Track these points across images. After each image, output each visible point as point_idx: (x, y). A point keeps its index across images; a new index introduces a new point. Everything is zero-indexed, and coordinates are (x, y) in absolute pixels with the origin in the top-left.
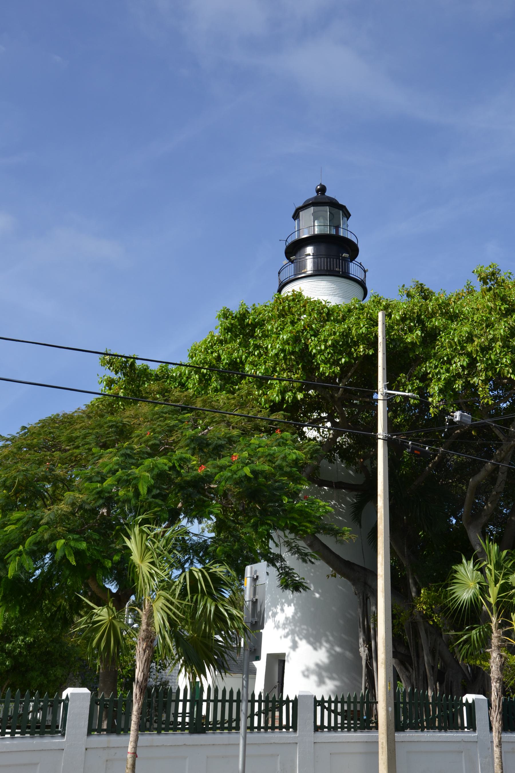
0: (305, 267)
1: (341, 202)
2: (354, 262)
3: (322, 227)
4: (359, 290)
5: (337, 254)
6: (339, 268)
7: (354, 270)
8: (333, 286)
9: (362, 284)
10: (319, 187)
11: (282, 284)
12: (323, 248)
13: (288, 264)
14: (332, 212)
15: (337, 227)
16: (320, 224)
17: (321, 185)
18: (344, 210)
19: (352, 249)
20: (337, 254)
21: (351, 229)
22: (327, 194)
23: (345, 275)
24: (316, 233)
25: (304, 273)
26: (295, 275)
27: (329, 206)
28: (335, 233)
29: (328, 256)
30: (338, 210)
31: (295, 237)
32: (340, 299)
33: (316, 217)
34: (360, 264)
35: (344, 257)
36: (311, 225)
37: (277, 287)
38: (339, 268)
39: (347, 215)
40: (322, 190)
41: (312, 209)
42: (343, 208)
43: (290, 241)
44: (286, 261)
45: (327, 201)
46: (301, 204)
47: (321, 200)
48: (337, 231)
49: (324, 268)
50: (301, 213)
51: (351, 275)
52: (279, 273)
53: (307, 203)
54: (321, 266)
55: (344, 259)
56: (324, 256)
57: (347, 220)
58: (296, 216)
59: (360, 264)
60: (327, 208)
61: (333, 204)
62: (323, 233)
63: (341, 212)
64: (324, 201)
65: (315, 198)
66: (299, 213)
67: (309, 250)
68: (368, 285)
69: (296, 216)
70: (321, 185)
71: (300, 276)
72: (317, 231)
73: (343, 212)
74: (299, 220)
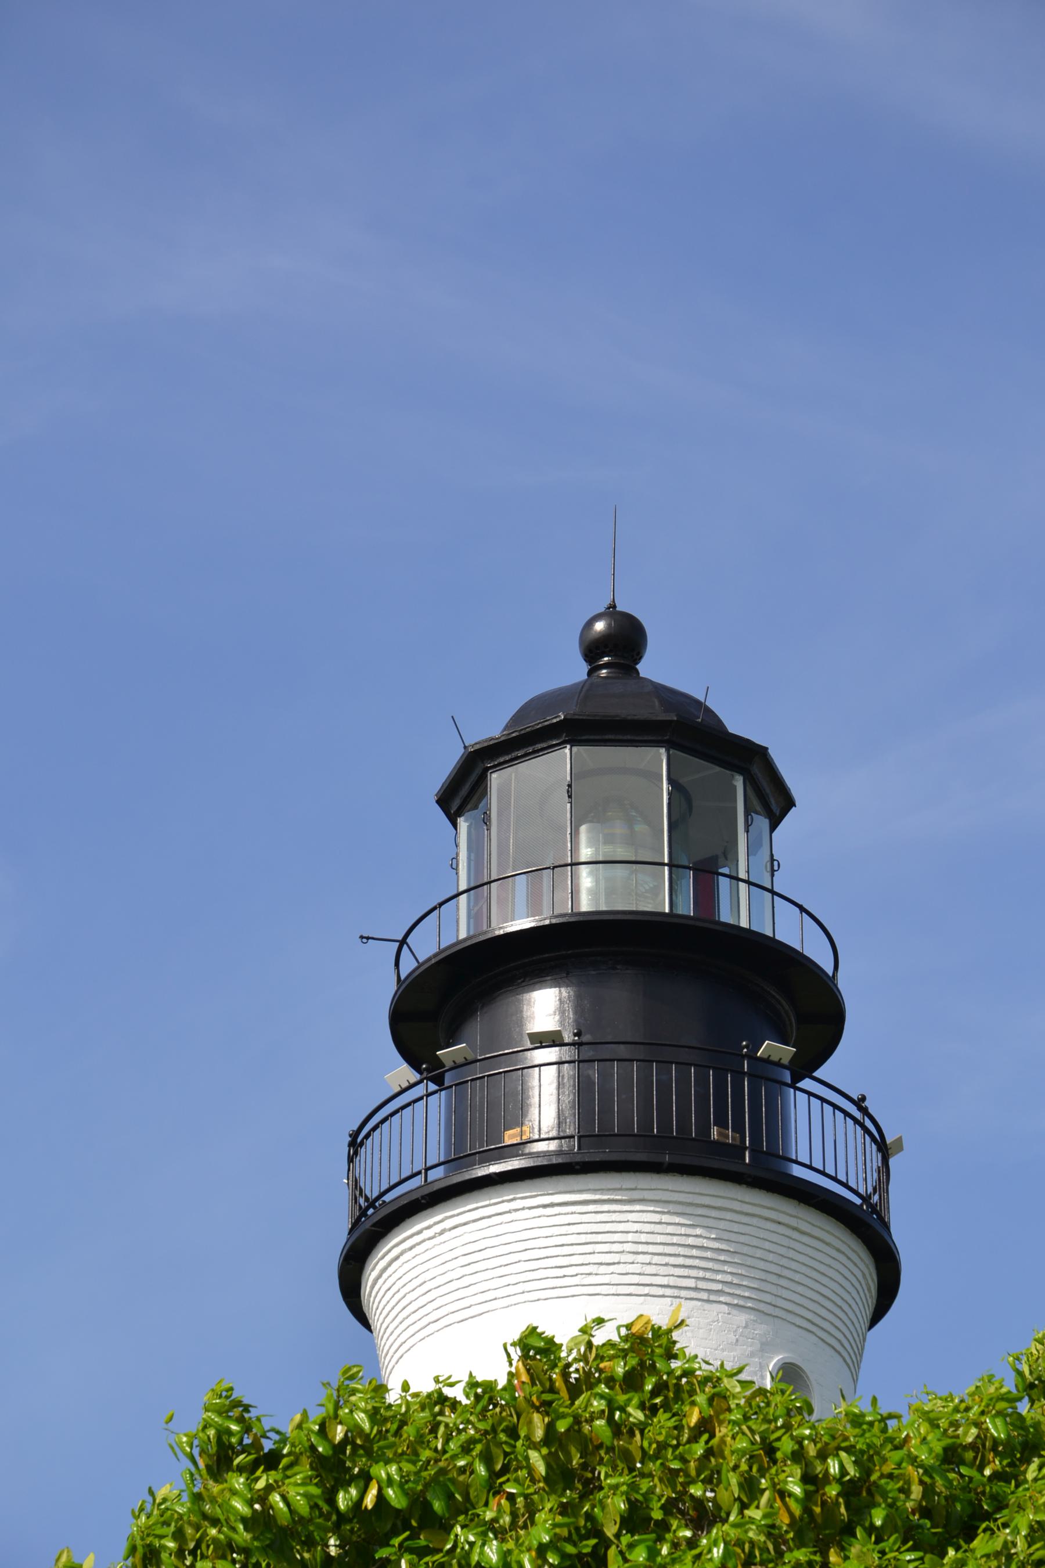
0: (517, 1109)
1: (736, 725)
2: (806, 1084)
3: (620, 872)
4: (849, 1265)
5: (708, 1041)
6: (739, 1128)
7: (815, 1138)
8: (699, 1236)
9: (865, 1225)
10: (600, 626)
11: (366, 1224)
12: (622, 994)
13: (419, 1091)
14: (683, 781)
15: (705, 869)
16: (621, 852)
17: (611, 611)
18: (756, 770)
19: (804, 1006)
20: (708, 1041)
21: (793, 887)
22: (651, 667)
23: (764, 1171)
24: (585, 905)
25: (514, 1150)
26: (452, 1162)
27: (669, 745)
28: (667, 910)
29: (654, 1050)
30: (726, 771)
31: (459, 927)
32: (741, 1318)
33: (585, 803)
34: (859, 1103)
35: (766, 1061)
36: (585, 852)
37: (336, 1235)
38: (739, 1128)
39: (774, 800)
40: (620, 643)
41: (560, 762)
42: (749, 760)
43: (426, 946)
44: (403, 1073)
45: (658, 713)
46: (491, 726)
47: (617, 704)
48: (706, 896)
49: (646, 1122)
50: (495, 779)
51: (797, 1171)
52: (356, 1143)
53: (536, 723)
54: (606, 1110)
55: (764, 1072)
56: (622, 1051)
57: (773, 827)
58: (463, 791)
59: (859, 1103)
60: (660, 758)
61: (693, 735)
62: (603, 908)
63: (739, 782)
64: (642, 713)
65: (585, 691)
66: (483, 778)
67: (544, 1007)
68: (902, 1233)
69: (463, 791)
70: (611, 611)
71: (495, 1168)
72: (594, 893)
73: (751, 781)
74: (486, 821)
